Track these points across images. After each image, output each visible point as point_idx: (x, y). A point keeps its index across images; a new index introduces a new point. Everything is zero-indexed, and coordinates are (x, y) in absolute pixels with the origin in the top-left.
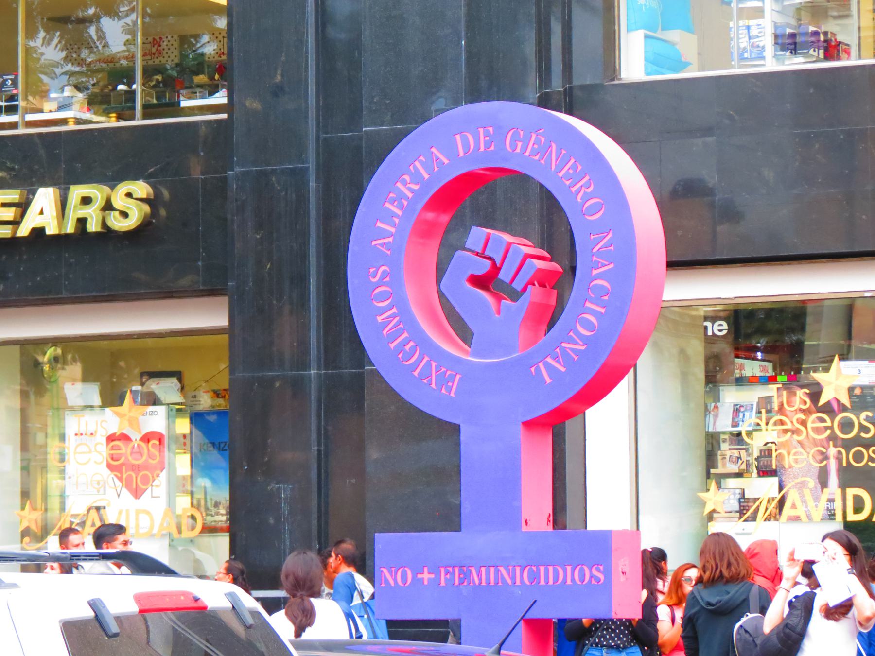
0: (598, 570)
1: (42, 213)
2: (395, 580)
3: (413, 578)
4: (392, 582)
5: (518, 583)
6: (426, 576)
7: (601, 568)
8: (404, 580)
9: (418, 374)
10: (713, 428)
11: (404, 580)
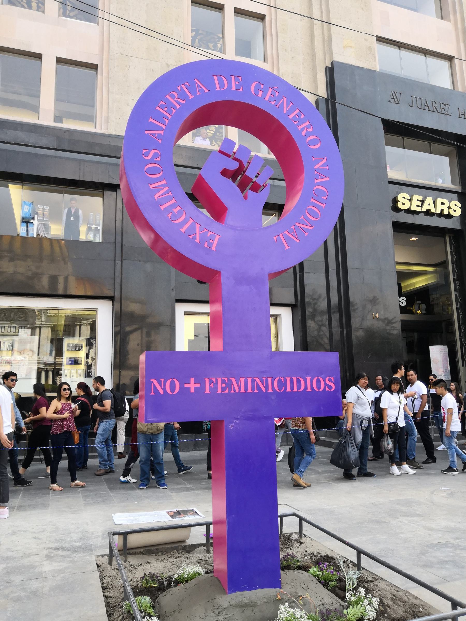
0: (330, 380)
1: (429, 205)
2: (164, 389)
3: (180, 388)
4: (161, 392)
5: (270, 390)
6: (192, 385)
7: (332, 378)
8: (173, 389)
9: (312, 202)
10: (318, 452)
11: (173, 389)
